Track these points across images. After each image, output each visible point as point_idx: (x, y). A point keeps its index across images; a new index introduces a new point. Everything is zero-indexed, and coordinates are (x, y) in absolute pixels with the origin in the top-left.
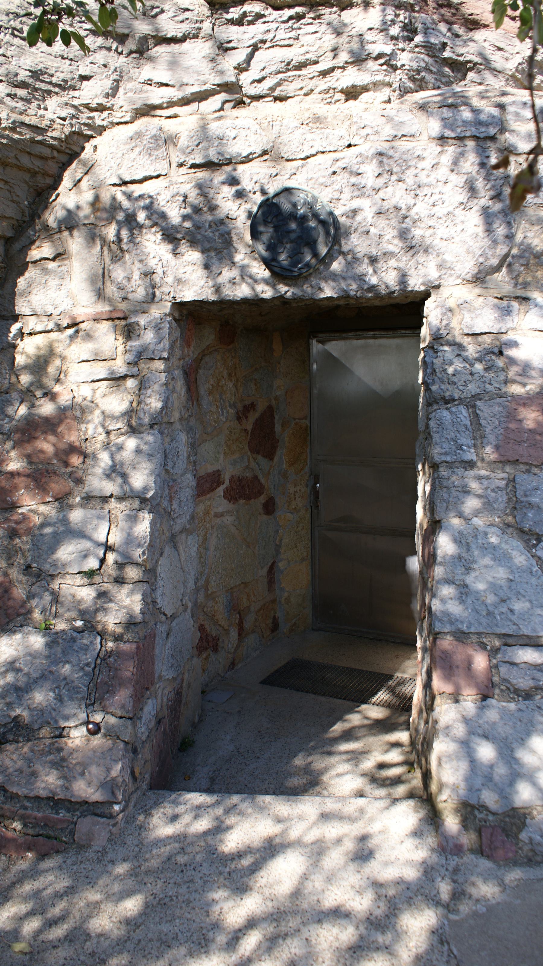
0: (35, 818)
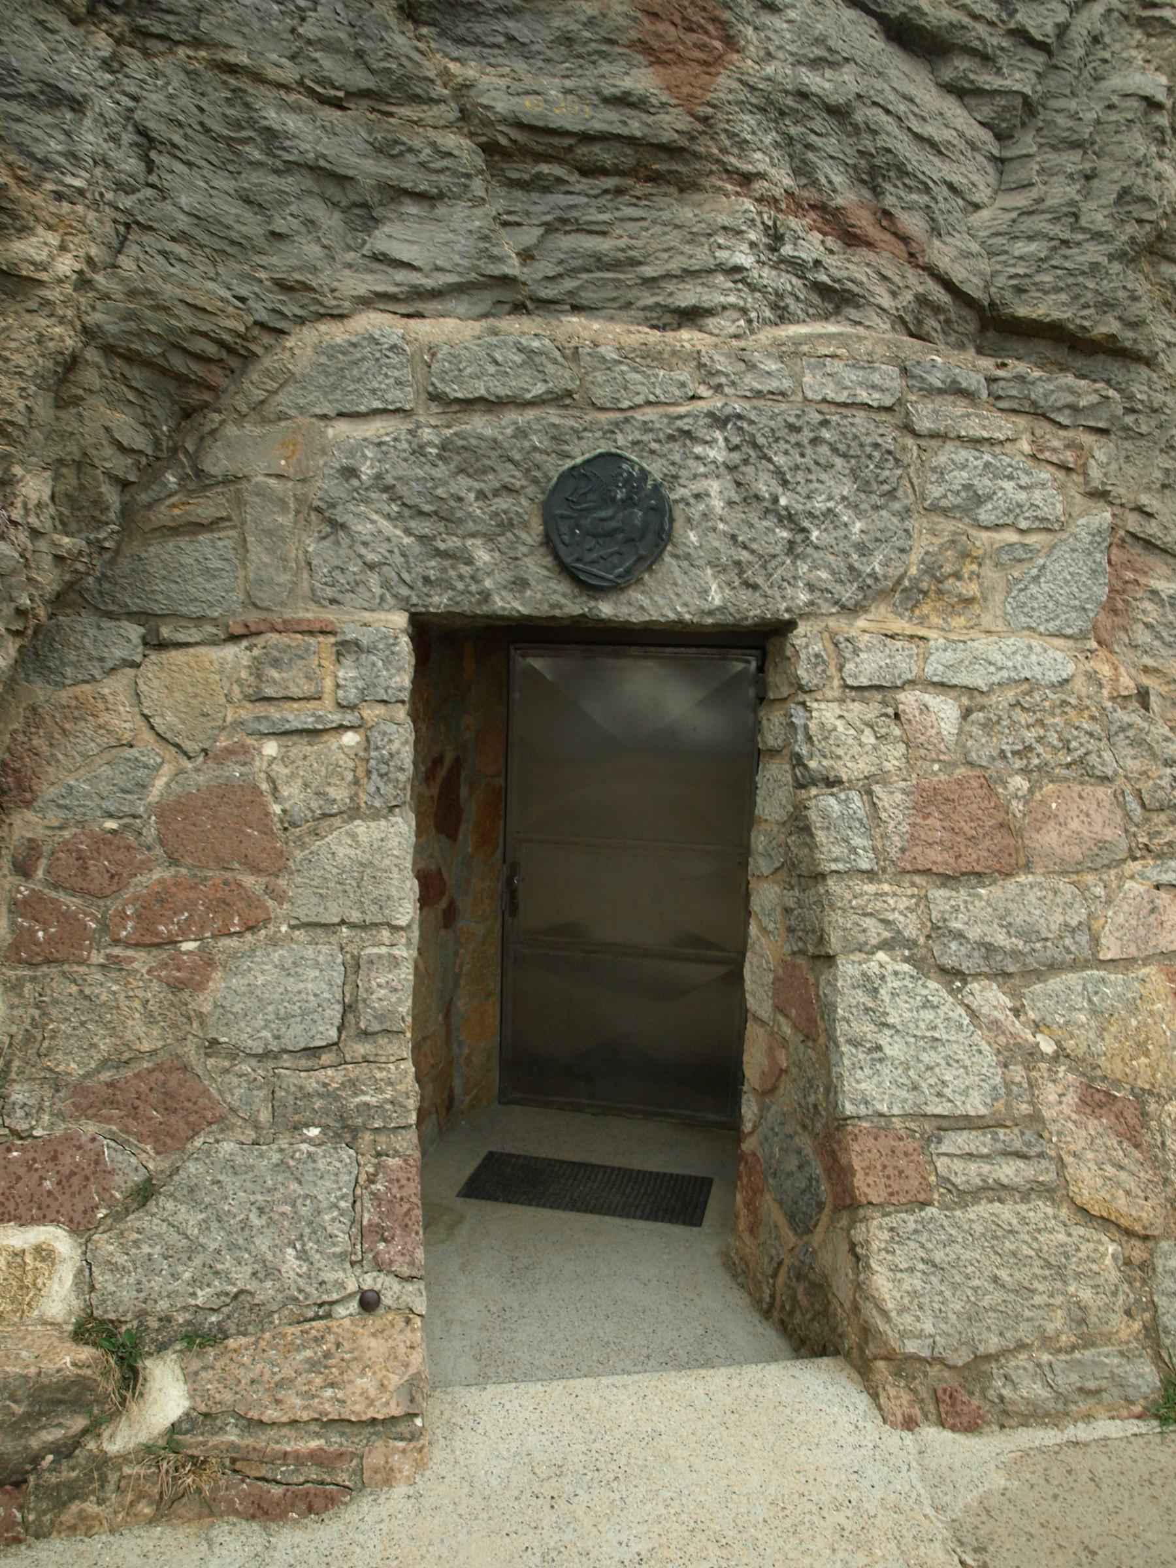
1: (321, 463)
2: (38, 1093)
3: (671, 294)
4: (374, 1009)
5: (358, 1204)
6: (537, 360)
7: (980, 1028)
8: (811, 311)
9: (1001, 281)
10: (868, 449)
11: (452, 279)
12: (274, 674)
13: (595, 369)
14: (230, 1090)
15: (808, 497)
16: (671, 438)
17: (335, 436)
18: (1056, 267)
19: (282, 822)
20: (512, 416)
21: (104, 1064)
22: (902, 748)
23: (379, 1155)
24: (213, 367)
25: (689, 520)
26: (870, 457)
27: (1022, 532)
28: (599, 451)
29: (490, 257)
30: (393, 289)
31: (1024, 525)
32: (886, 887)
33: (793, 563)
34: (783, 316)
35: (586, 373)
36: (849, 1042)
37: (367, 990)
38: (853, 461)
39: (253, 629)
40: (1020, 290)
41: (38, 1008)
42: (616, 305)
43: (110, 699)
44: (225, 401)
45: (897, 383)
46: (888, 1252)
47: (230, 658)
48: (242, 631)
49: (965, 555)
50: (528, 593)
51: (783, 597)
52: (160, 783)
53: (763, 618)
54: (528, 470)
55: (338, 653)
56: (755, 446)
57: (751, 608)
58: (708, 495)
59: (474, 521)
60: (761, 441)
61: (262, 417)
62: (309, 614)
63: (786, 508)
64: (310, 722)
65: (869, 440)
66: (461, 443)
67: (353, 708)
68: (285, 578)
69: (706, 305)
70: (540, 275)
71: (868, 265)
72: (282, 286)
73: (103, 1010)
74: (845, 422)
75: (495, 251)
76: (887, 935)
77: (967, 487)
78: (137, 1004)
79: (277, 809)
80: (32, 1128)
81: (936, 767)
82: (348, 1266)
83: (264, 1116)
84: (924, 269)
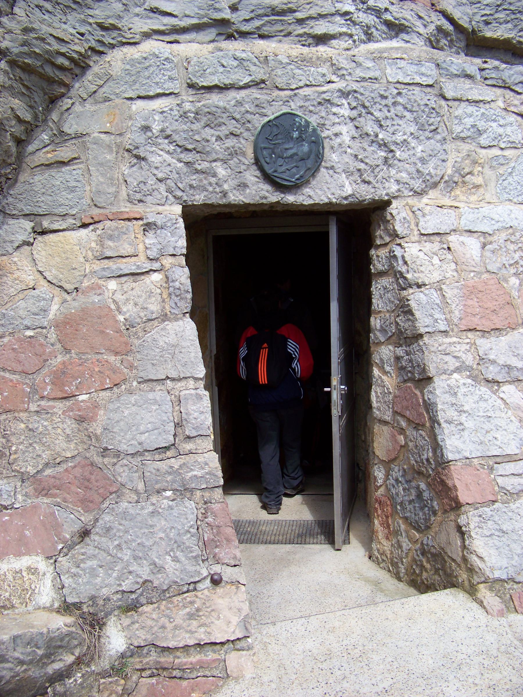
0: (191, 664)
1: (130, 124)
2: (12, 485)
3: (312, 27)
4: (193, 424)
5: (200, 529)
6: (245, 64)
7: (510, 409)
8: (384, 36)
9: (478, 18)
10: (422, 108)
11: (195, 21)
12: (110, 243)
13: (276, 68)
14: (119, 474)
15: (393, 134)
16: (320, 103)
17: (137, 109)
18: (505, 10)
19: (125, 325)
20: (233, 94)
21: (47, 465)
22: (453, 266)
23: (206, 503)
24: (67, 73)
25: (332, 148)
26: (423, 111)
27: (502, 149)
28: (281, 112)
29: (215, 9)
30: (163, 28)
31: (503, 146)
32: (455, 339)
33: (388, 169)
34: (369, 38)
35: (272, 70)
36: (446, 421)
37: (186, 414)
38: (415, 114)
39: (96, 219)
40: (487, 23)
41: (4, 438)
42: (283, 34)
43: (19, 263)
44: (73, 92)
45: (434, 72)
46: (479, 528)
47: (84, 236)
48: (91, 221)
49: (475, 162)
50: (248, 191)
51: (384, 188)
52: (55, 307)
53: (374, 200)
54: (244, 123)
55: (144, 230)
56: (364, 107)
57: (367, 194)
58: (342, 134)
59: (216, 153)
60: (367, 104)
61: (95, 100)
62: (126, 208)
63: (383, 140)
64: (134, 269)
65: (422, 103)
66: (207, 110)
67: (156, 260)
68: (112, 190)
69: (331, 33)
70: (241, 19)
71: (412, 10)
72: (102, 27)
73: (41, 436)
74: (410, 93)
75: (217, 6)
76: (457, 364)
77: (473, 126)
78: (59, 431)
79: (121, 318)
80: (14, 503)
81: (472, 274)
82: (201, 562)
83: (141, 486)
84: (440, 12)
